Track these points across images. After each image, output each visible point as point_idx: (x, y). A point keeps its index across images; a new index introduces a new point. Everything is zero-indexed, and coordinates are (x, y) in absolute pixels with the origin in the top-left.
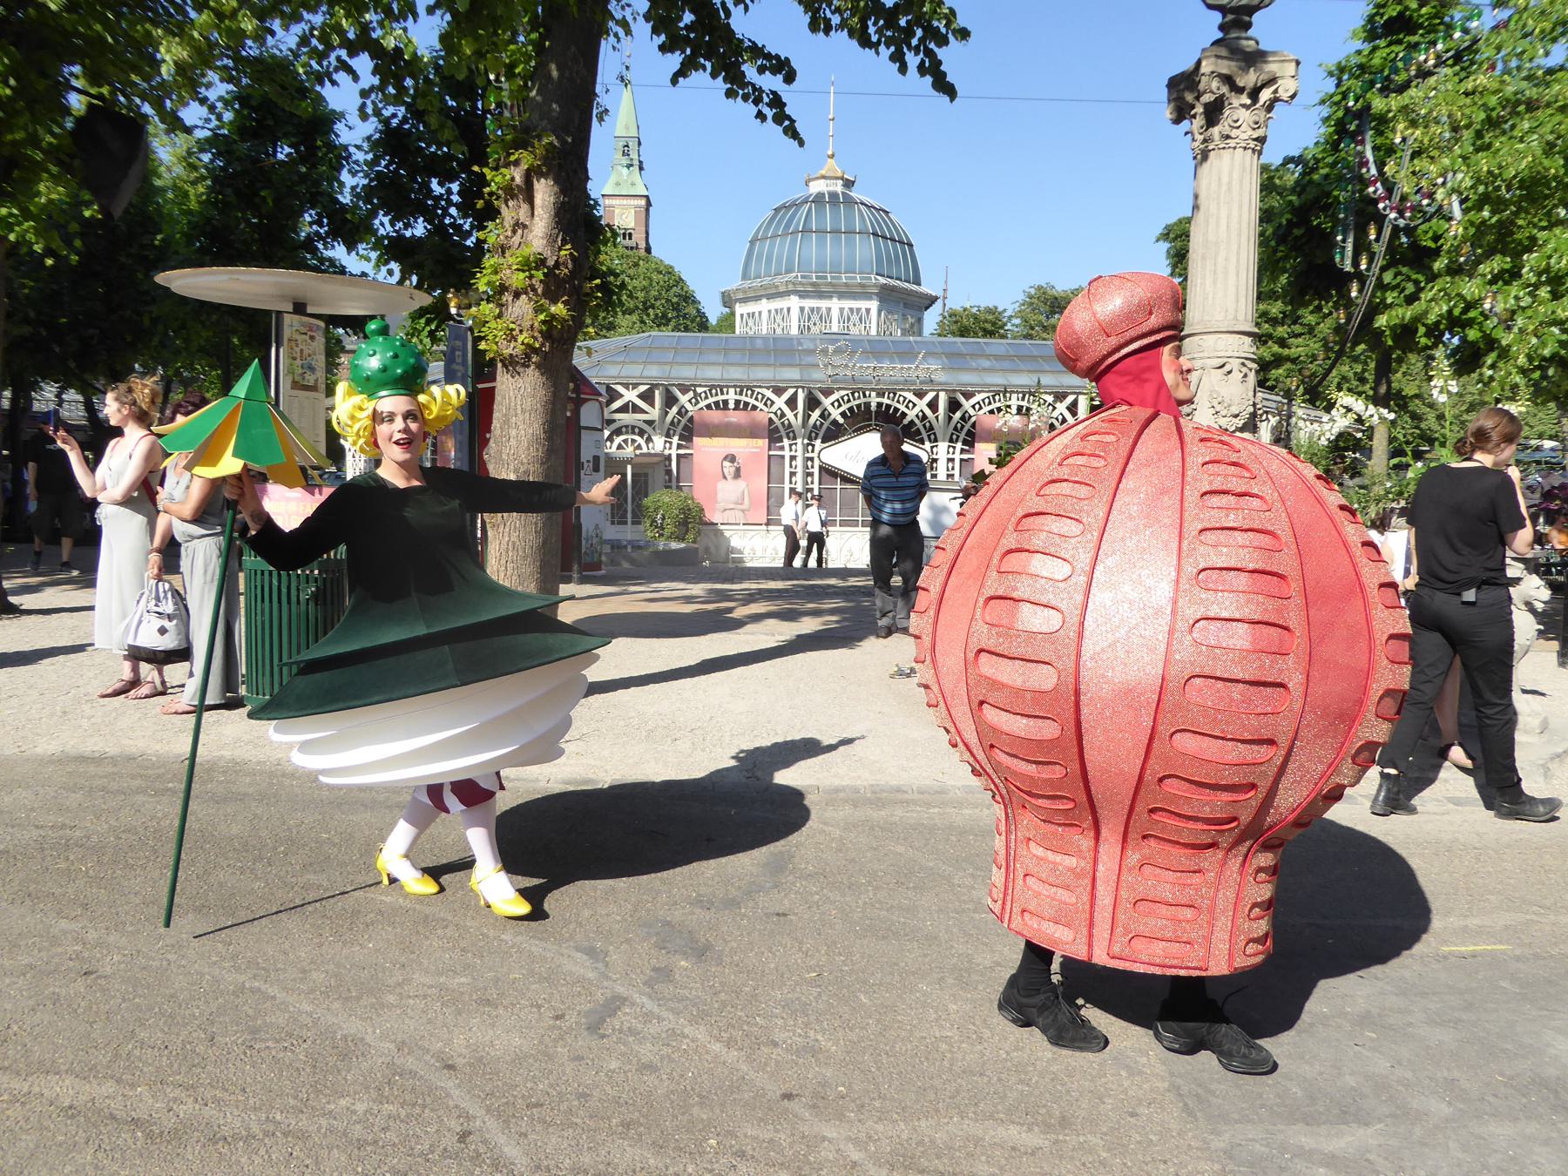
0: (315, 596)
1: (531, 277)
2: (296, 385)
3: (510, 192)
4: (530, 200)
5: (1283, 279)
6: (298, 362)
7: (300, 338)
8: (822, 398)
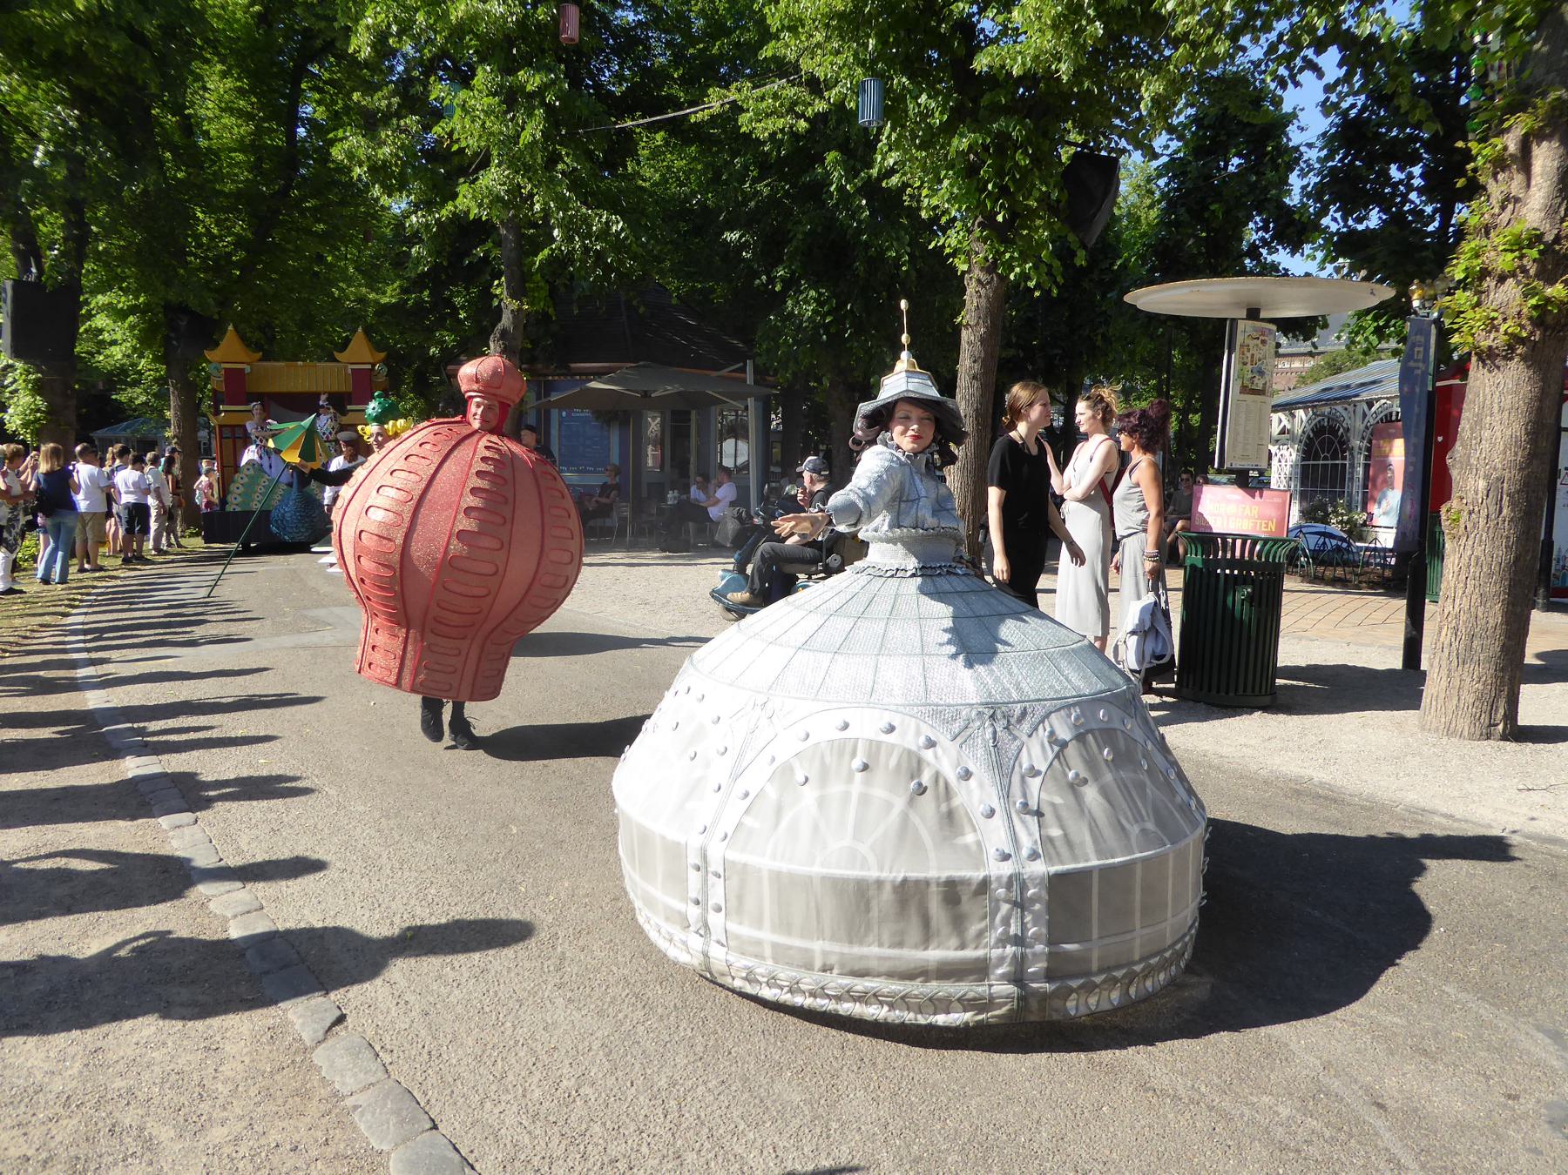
0: (1251, 598)
1: (1522, 257)
2: (1245, 390)
3: (1500, 164)
4: (1526, 168)
5: (479, 252)
6: (1249, 367)
7: (1252, 343)
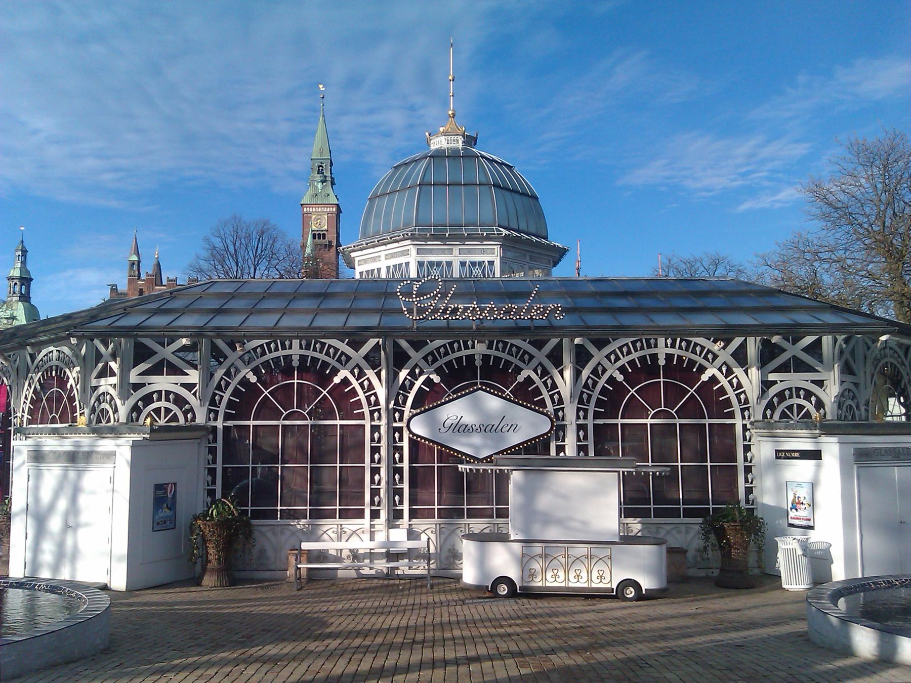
8: (411, 352)
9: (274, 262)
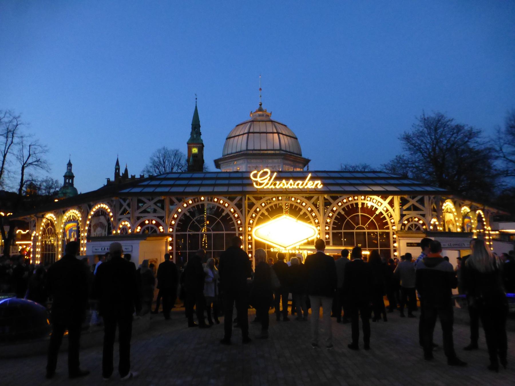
9: (180, 167)
